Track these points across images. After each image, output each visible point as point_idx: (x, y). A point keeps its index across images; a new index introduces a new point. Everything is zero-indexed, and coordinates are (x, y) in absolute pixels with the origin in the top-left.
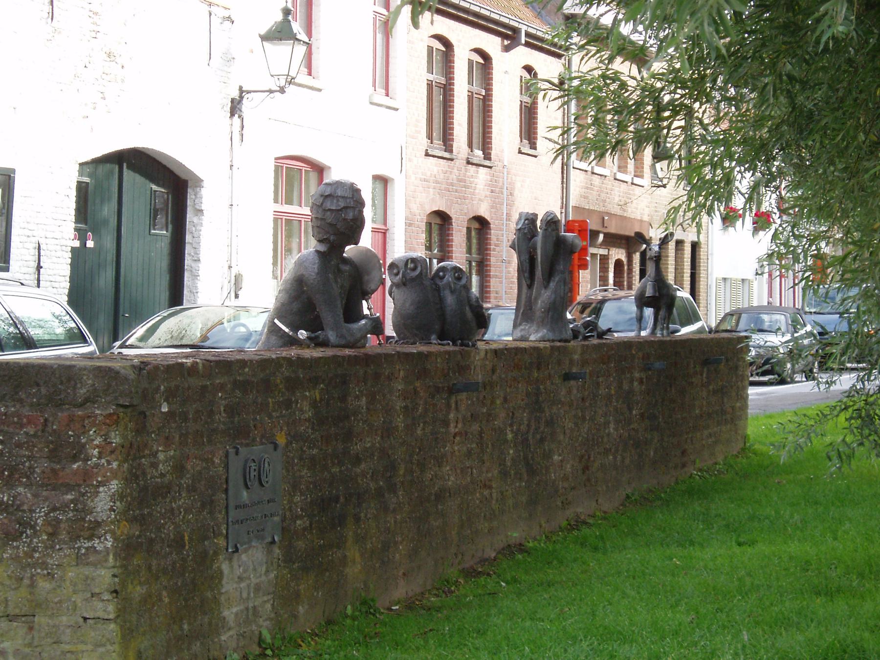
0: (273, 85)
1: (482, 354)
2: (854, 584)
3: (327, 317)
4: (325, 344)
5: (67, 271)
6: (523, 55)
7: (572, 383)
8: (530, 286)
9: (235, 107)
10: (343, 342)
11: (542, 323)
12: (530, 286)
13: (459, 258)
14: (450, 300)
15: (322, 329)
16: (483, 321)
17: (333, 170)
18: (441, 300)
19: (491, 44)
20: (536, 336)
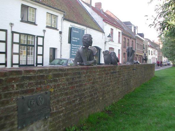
0: (108, 41)
1: (118, 67)
2: (113, 101)
3: (84, 60)
4: (83, 65)
5: (104, 60)
6: (132, 40)
7: (134, 70)
8: (129, 57)
9: (105, 43)
10: (87, 65)
11: (130, 62)
12: (129, 57)
13: (76, 52)
14: (113, 58)
15: (83, 62)
16: (118, 61)
17: (58, 49)
18: (111, 58)
19: (129, 39)
20: (129, 64)
